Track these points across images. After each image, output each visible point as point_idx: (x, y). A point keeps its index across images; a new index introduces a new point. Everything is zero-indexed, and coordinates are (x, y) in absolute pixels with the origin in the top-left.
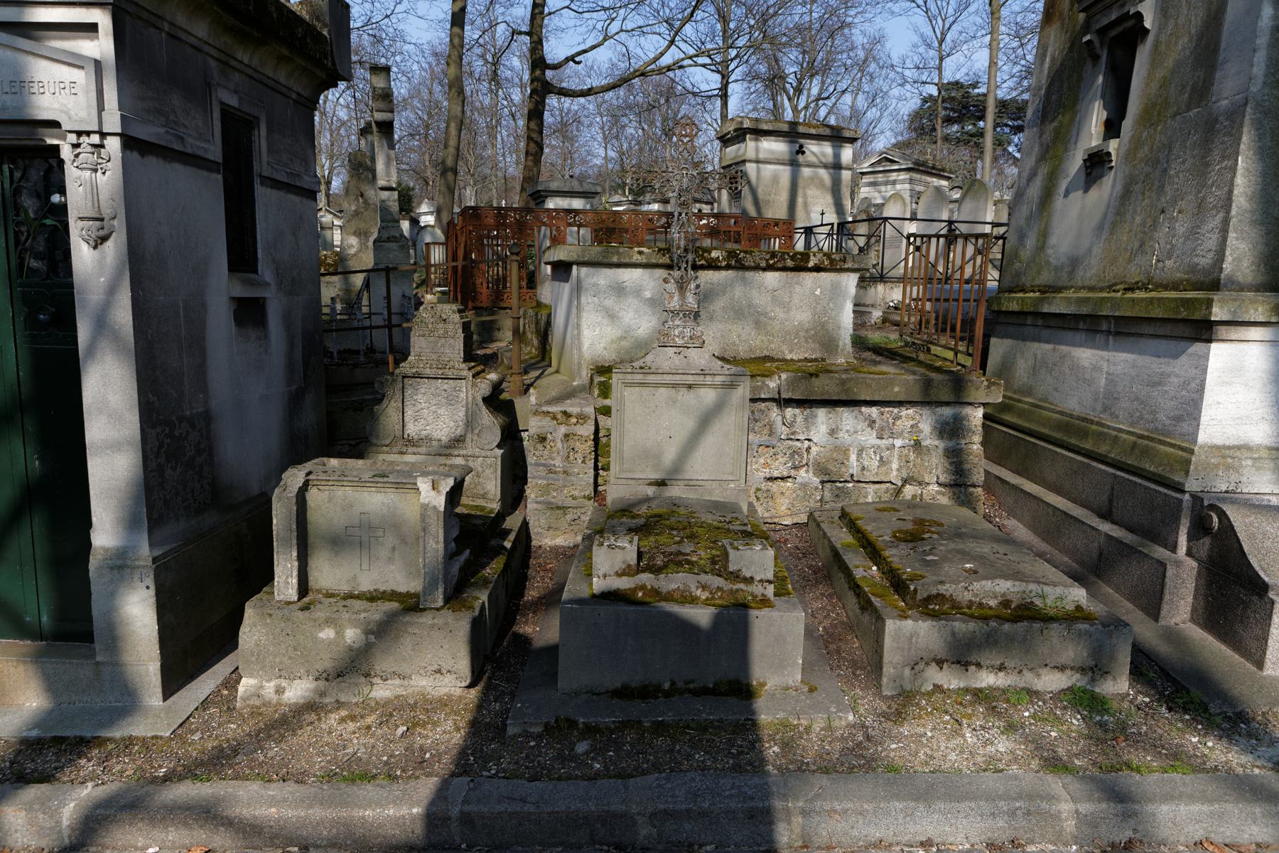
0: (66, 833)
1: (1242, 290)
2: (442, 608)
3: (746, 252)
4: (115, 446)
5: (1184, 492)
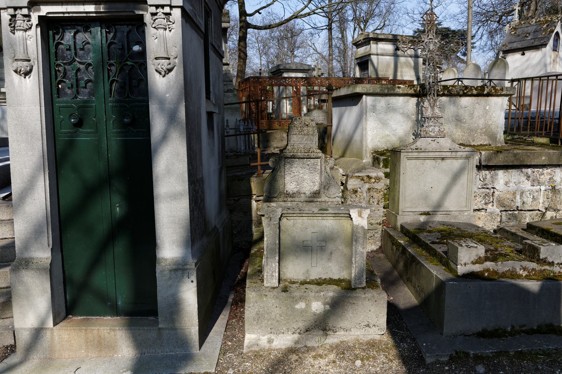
4: (174, 197)
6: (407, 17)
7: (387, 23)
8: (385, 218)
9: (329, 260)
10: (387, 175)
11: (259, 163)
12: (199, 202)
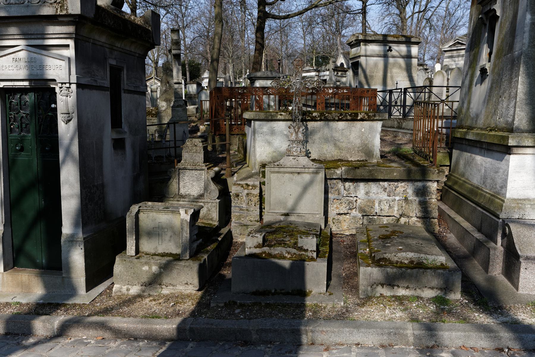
0: (56, 330)
1: (523, 132)
2: (188, 259)
3: (328, 113)
4: (72, 196)
5: (499, 218)
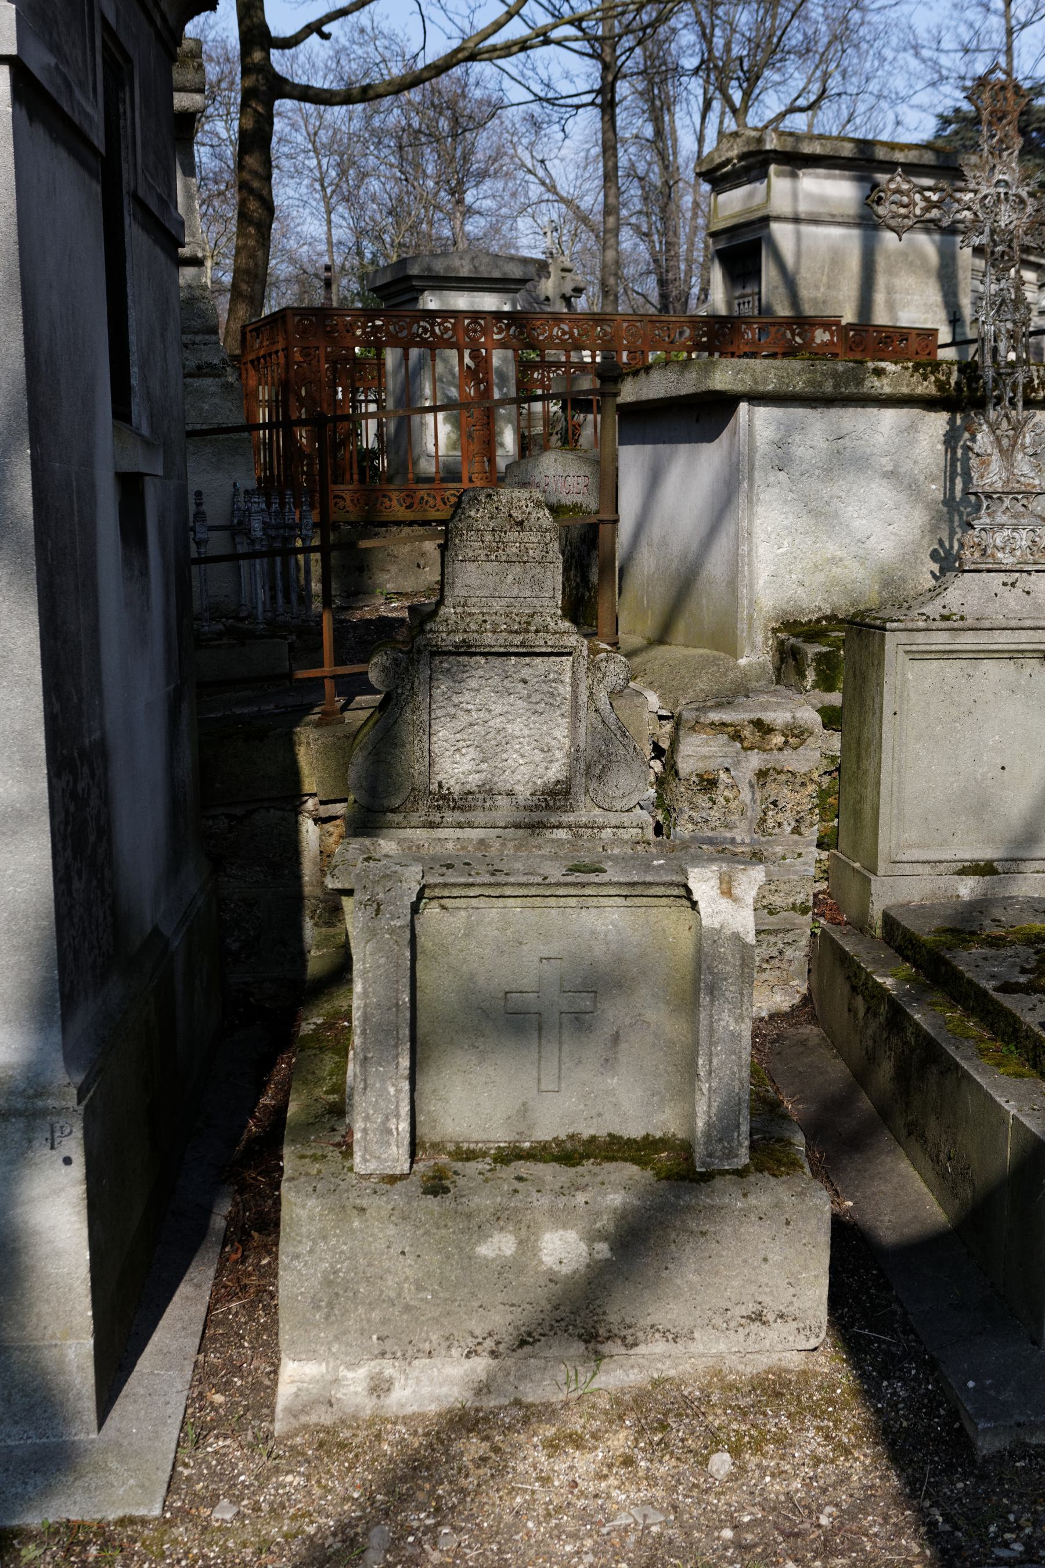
6: (914, 64)
7: (834, 84)
8: (823, 886)
9: (608, 1063)
10: (831, 718)
11: (328, 669)
12: (92, 838)
